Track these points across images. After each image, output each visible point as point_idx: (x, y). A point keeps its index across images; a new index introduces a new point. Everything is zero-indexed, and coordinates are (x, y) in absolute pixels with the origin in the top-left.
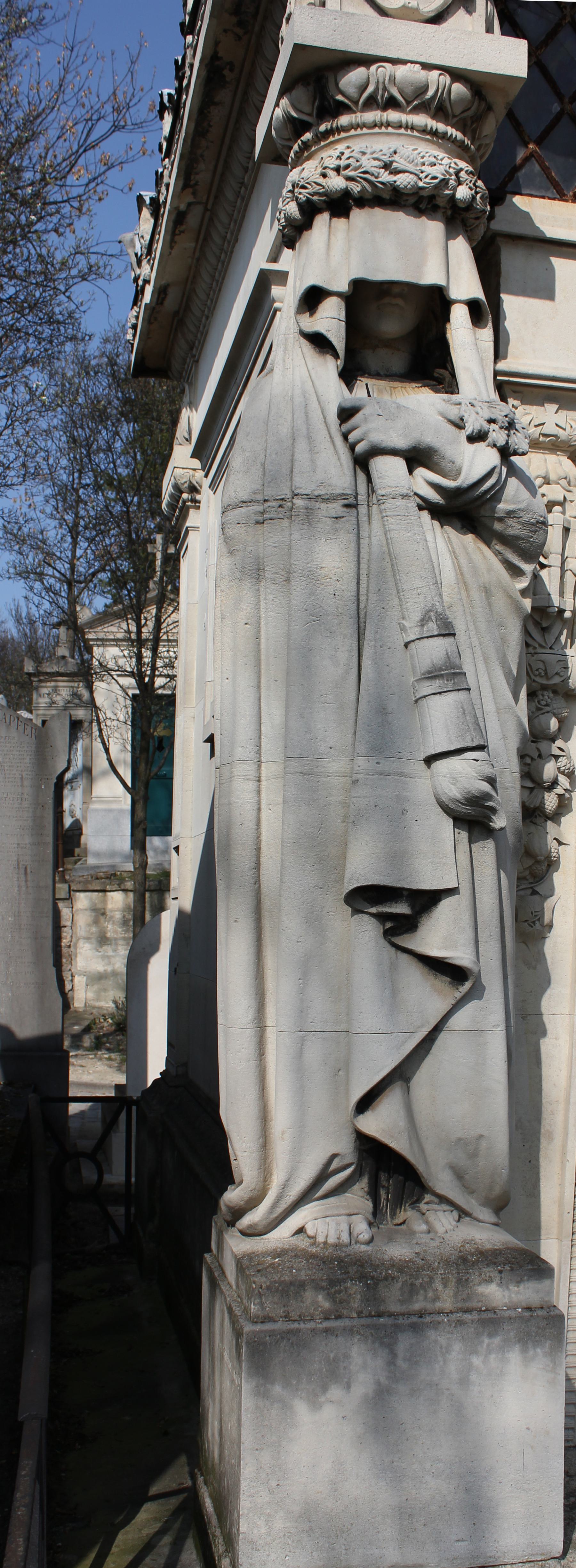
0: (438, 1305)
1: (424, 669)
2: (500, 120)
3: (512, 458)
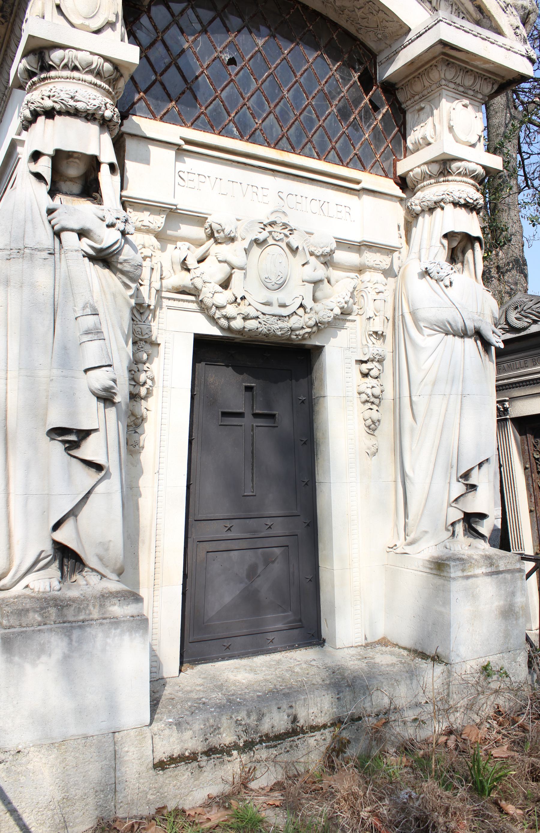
0: (91, 616)
1: (84, 330)
2: (127, 81)
3: (127, 236)
